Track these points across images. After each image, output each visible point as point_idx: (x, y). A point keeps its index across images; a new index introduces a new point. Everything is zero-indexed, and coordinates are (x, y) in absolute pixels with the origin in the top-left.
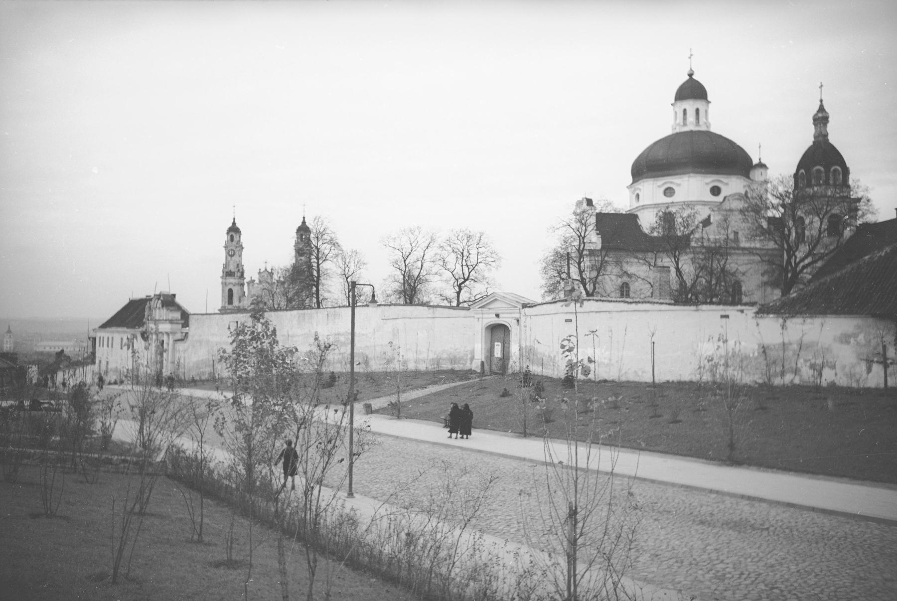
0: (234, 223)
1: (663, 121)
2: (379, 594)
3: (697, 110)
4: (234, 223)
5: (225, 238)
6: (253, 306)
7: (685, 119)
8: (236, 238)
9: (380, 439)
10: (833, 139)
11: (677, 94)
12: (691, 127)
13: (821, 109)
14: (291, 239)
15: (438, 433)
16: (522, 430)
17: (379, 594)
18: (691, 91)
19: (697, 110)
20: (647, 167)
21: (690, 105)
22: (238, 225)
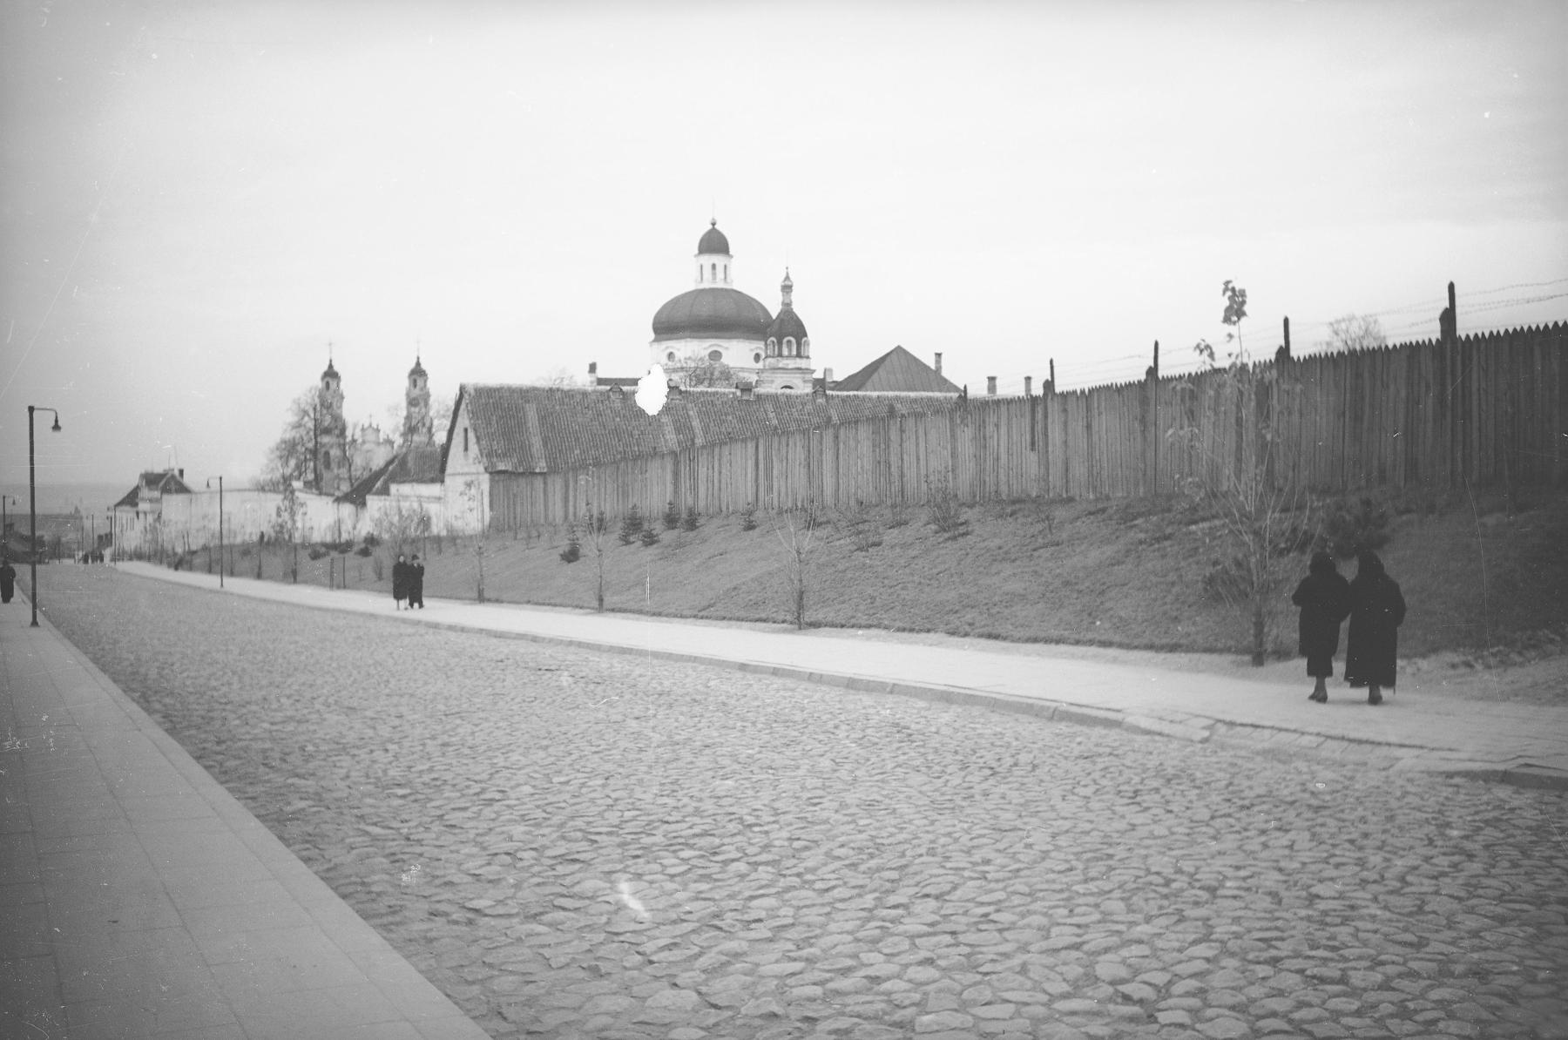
0: (331, 366)
1: (684, 275)
2: (873, 598)
3: (714, 266)
4: (331, 366)
5: (405, 383)
6: (292, 463)
7: (714, 274)
8: (333, 385)
9: (1449, 414)
10: (796, 309)
11: (702, 241)
12: (706, 285)
13: (787, 278)
14: (986, 383)
15: (384, 604)
16: (475, 595)
17: (873, 598)
18: (714, 243)
19: (714, 266)
20: (668, 326)
21: (708, 260)
22: (336, 368)
